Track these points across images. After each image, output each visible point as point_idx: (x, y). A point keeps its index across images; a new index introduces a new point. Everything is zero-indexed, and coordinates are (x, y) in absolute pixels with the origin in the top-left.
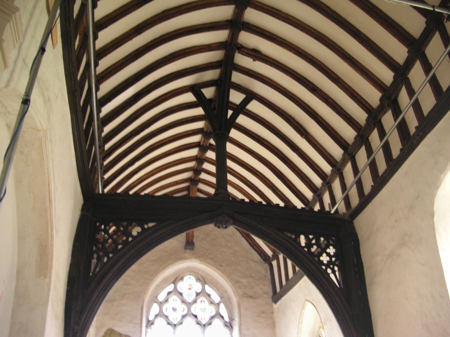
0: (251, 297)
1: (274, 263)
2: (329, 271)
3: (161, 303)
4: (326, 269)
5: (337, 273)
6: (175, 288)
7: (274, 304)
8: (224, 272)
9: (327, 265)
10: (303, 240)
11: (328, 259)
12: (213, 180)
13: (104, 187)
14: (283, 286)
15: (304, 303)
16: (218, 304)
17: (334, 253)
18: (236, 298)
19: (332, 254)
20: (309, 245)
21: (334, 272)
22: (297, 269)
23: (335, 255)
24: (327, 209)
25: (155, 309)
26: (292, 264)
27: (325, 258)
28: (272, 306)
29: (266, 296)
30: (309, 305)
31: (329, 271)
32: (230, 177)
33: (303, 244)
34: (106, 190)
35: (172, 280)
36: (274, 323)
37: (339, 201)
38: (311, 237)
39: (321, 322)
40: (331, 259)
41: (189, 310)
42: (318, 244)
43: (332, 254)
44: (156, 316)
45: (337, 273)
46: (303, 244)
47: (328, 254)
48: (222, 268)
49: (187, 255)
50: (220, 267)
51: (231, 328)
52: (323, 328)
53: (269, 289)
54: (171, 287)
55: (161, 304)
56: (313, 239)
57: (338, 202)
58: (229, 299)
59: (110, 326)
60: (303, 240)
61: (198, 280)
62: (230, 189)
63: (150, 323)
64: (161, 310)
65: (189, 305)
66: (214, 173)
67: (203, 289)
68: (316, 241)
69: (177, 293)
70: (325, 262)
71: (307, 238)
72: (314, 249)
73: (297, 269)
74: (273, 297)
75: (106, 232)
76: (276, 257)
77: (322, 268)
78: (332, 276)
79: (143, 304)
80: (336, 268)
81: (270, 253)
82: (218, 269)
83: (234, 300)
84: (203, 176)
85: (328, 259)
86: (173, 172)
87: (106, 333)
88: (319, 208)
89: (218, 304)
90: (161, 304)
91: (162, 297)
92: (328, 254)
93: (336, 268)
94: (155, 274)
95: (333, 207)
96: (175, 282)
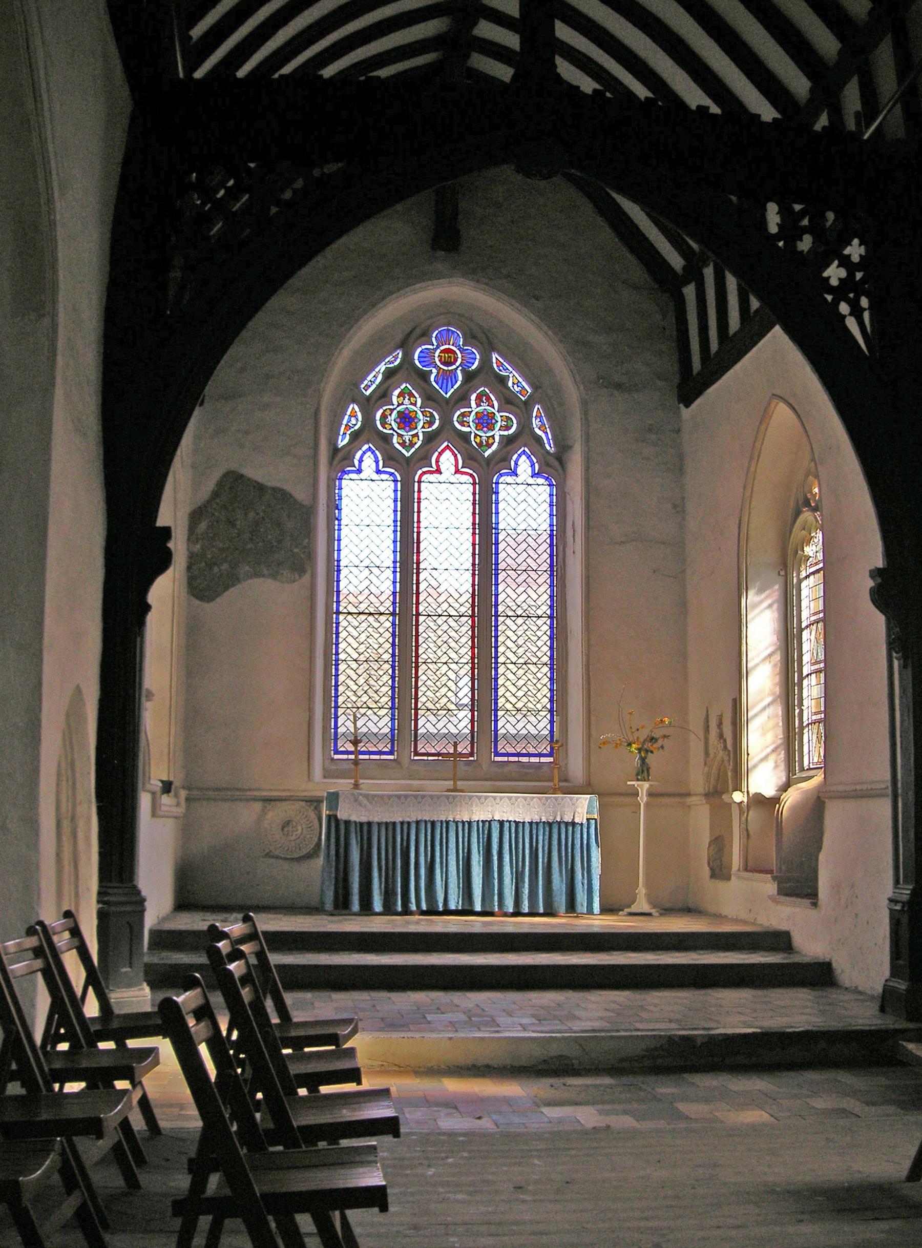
0: (618, 386)
1: (690, 291)
2: (844, 308)
3: (368, 399)
4: (836, 303)
5: (866, 316)
6: (408, 358)
7: (681, 406)
8: (545, 317)
9: (841, 292)
10: (773, 218)
11: (843, 273)
12: (512, 40)
13: (191, 67)
14: (712, 356)
15: (769, 404)
16: (527, 406)
17: (860, 255)
18: (578, 388)
19: (856, 259)
20: (791, 230)
21: (857, 312)
22: (755, 304)
23: (864, 263)
24: (851, 125)
25: (354, 416)
26: (739, 285)
27: (834, 273)
28: (678, 413)
29: (660, 383)
30: (782, 411)
31: (844, 308)
32: (563, 31)
33: (773, 229)
34: (198, 74)
35: (399, 337)
36: (681, 457)
37: (887, 105)
38: (797, 207)
39: (813, 460)
40: (851, 275)
41: (446, 422)
42: (816, 230)
43: (856, 259)
44: (355, 436)
45: (866, 316)
46: (773, 229)
47: (845, 262)
48: (539, 304)
49: (439, 266)
50: (533, 301)
51: (560, 471)
52: (817, 476)
53: (672, 366)
54: (396, 359)
55: (368, 405)
56: (803, 214)
57: (884, 108)
58: (558, 389)
59: (233, 466)
60: (773, 218)
61: (471, 337)
62: (566, 70)
63: (340, 455)
64: (368, 420)
65: (446, 407)
66: (514, 18)
67: (486, 362)
68: (810, 221)
69: (412, 374)
70: (834, 282)
71: (784, 211)
72: (805, 244)
73: (755, 304)
74: (680, 387)
75: (207, 193)
76: (693, 273)
77: (826, 300)
78: (852, 324)
79: (319, 405)
80: (864, 302)
81: (676, 261)
82: (526, 304)
83: (572, 393)
84: (486, 30)
85: (843, 273)
86: (388, 53)
87: (220, 484)
88: (827, 124)
89: (525, 403)
90: (368, 405)
91: (373, 380)
92: (845, 262)
93: (864, 302)
94: (351, 319)
95: (868, 126)
96: (406, 344)
